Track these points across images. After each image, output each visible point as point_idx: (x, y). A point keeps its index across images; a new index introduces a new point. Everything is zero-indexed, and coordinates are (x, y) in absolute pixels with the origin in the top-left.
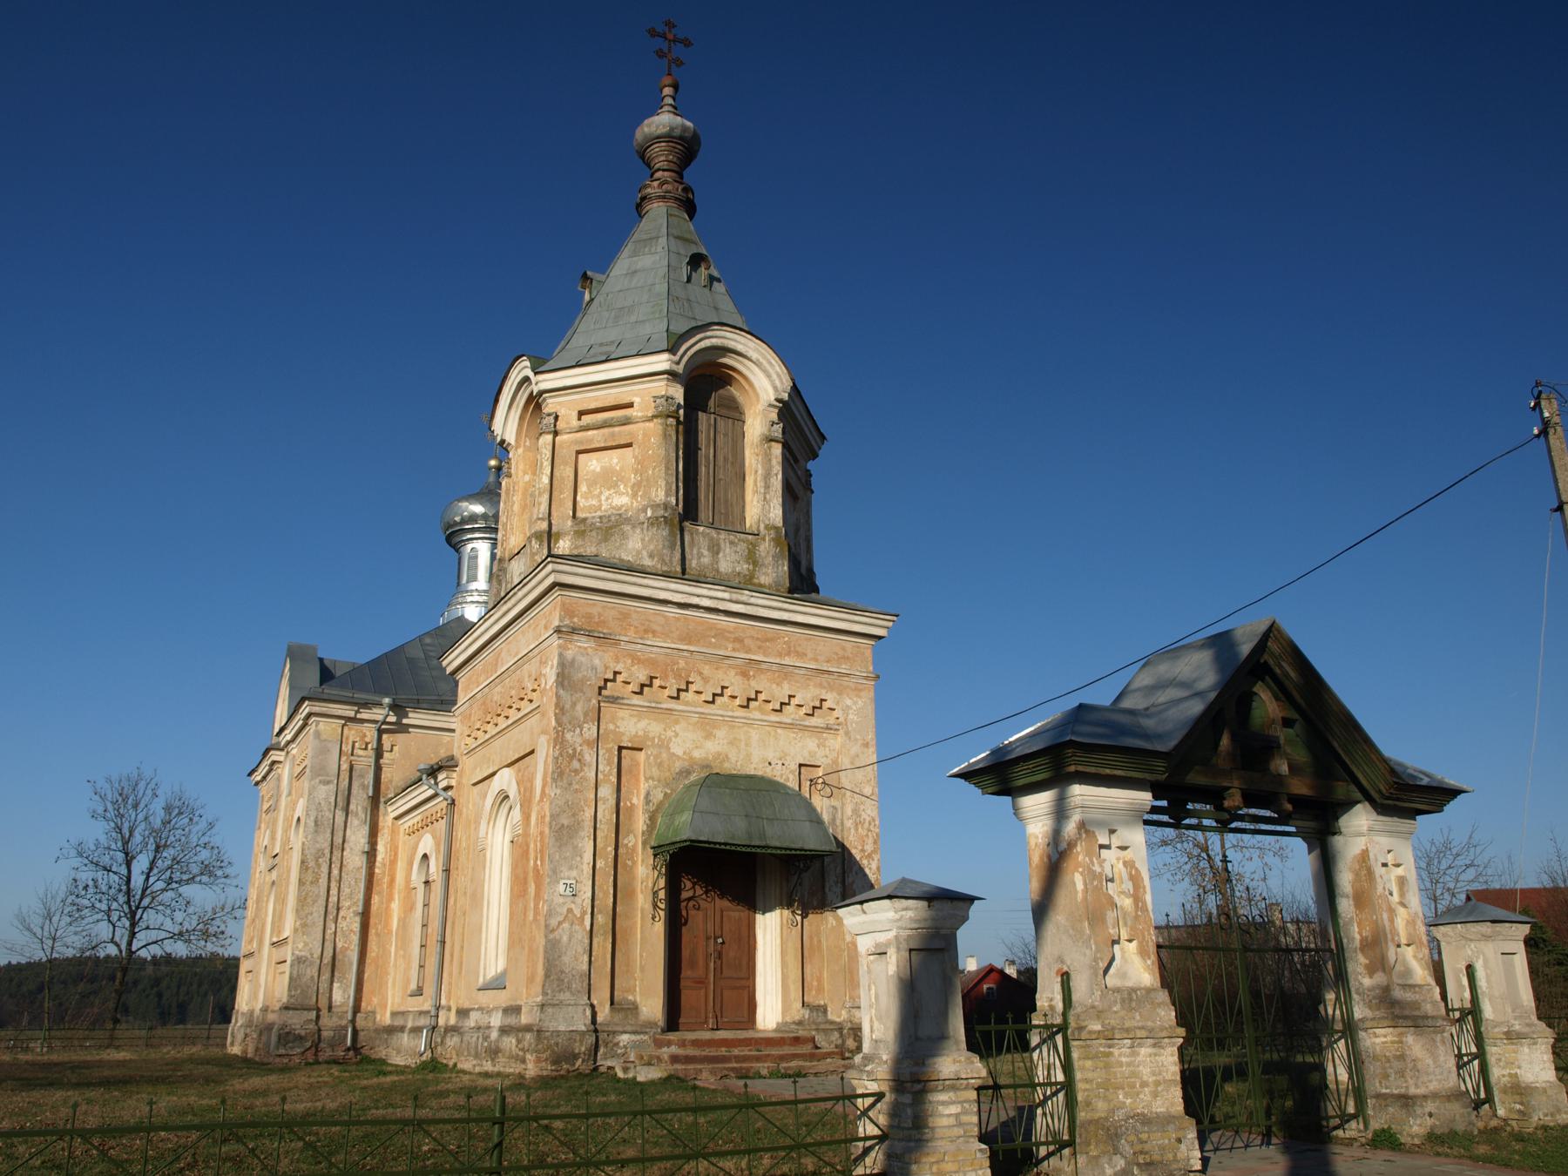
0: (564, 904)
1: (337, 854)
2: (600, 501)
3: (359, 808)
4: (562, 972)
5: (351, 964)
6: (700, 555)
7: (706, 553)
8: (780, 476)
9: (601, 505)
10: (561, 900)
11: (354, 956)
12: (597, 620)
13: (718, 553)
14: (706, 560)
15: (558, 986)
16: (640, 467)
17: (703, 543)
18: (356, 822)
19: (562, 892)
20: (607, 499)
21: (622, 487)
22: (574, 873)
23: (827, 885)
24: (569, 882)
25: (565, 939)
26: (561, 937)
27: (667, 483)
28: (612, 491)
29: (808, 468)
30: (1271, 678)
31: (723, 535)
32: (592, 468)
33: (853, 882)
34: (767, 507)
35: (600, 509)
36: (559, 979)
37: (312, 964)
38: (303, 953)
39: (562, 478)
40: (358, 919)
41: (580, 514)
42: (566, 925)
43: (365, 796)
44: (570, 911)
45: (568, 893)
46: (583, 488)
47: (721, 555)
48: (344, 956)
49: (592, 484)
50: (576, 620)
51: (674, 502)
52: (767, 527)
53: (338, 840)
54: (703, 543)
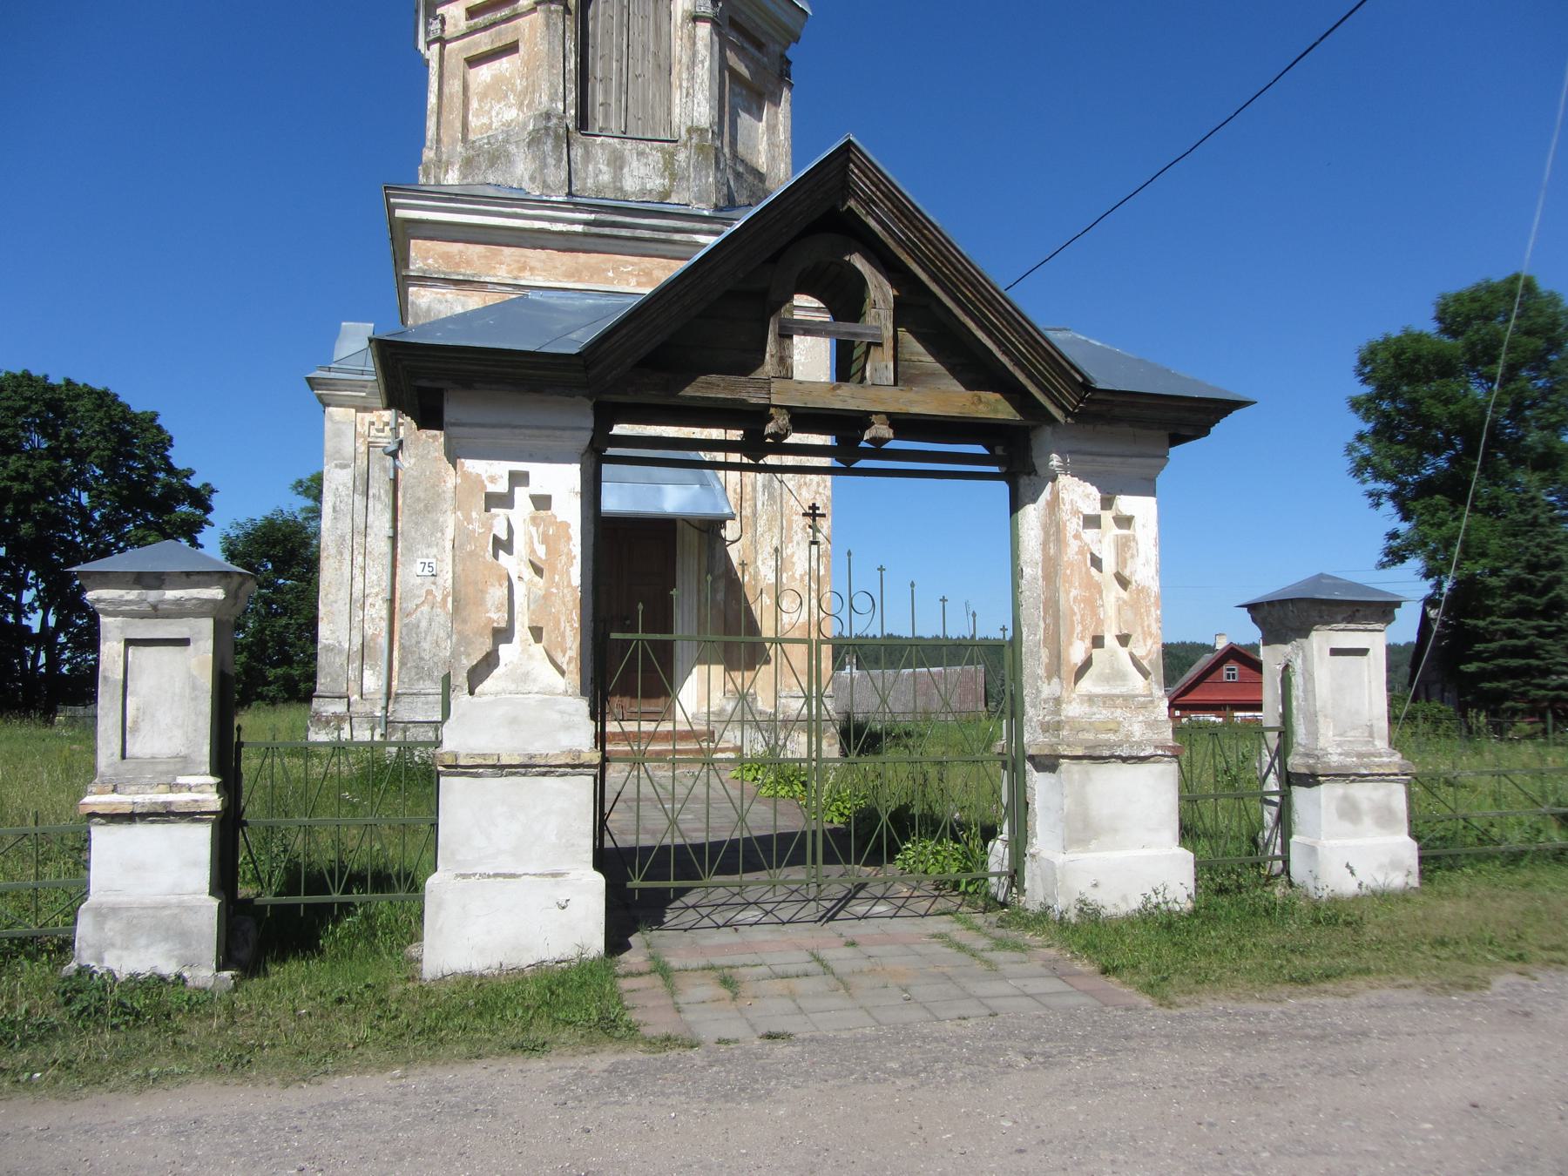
0: (422, 584)
1: (358, 539)
2: (491, 118)
3: (382, 491)
4: (421, 659)
5: (382, 652)
6: (598, 173)
7: (604, 168)
8: (707, 64)
9: (491, 124)
10: (419, 580)
11: (383, 641)
12: (457, 260)
13: (621, 168)
14: (605, 178)
15: (417, 674)
16: (530, 70)
17: (601, 157)
18: (379, 506)
19: (420, 573)
20: (498, 114)
21: (512, 97)
22: (434, 551)
23: (760, 557)
24: (427, 561)
25: (424, 624)
26: (419, 621)
27: (552, 85)
28: (503, 103)
29: (789, 54)
30: (394, 198)
31: (629, 145)
32: (483, 78)
33: (792, 555)
34: (690, 104)
35: (491, 129)
36: (417, 667)
37: (341, 652)
38: (331, 642)
39: (451, 95)
40: (385, 606)
41: (472, 137)
42: (425, 608)
43: (387, 479)
44: (429, 592)
45: (426, 572)
46: (474, 104)
47: (626, 170)
48: (376, 644)
49: (483, 96)
50: (430, 261)
51: (562, 108)
52: (690, 130)
53: (360, 521)
54: (601, 157)
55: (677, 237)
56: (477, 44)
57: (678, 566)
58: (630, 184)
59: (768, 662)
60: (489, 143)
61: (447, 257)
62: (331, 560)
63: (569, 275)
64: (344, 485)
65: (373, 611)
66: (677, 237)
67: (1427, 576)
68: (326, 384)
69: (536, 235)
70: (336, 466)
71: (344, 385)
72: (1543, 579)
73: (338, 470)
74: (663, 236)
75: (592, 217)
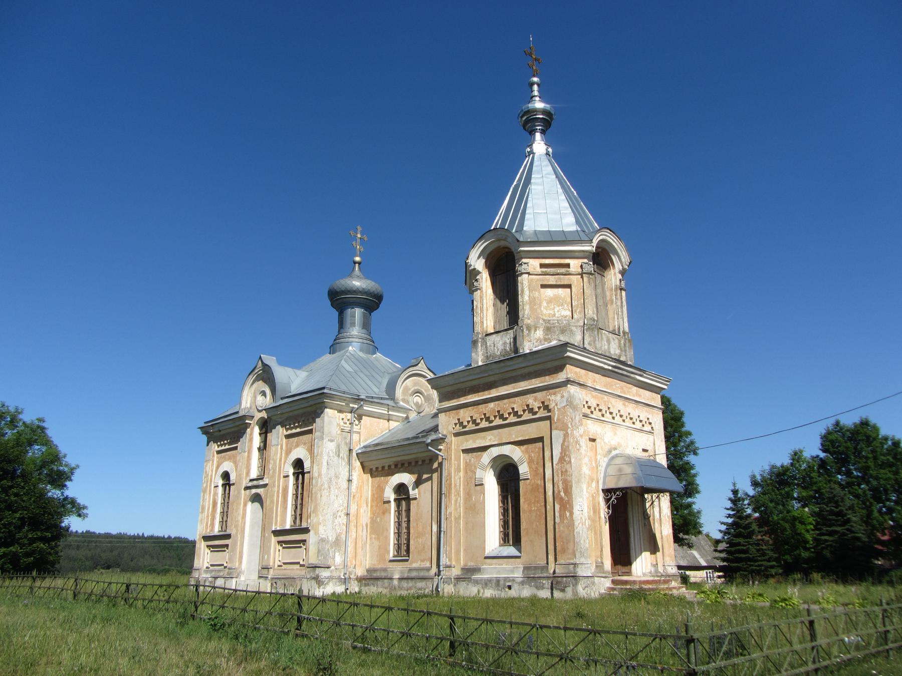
25: (581, 532)
48: (340, 538)
55: (632, 375)
56: (548, 280)
57: (630, 509)
58: (612, 352)
59: (659, 551)
60: (558, 323)
61: (576, 373)
62: (325, 491)
63: (605, 386)
64: (332, 451)
65: (340, 520)
66: (632, 375)
67: (65, 486)
68: (330, 397)
69: (600, 369)
70: (329, 440)
71: (338, 398)
72: (847, 527)
73: (329, 442)
74: (629, 374)
75: (614, 364)
